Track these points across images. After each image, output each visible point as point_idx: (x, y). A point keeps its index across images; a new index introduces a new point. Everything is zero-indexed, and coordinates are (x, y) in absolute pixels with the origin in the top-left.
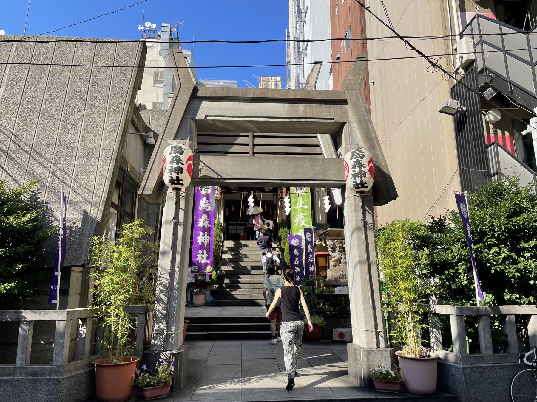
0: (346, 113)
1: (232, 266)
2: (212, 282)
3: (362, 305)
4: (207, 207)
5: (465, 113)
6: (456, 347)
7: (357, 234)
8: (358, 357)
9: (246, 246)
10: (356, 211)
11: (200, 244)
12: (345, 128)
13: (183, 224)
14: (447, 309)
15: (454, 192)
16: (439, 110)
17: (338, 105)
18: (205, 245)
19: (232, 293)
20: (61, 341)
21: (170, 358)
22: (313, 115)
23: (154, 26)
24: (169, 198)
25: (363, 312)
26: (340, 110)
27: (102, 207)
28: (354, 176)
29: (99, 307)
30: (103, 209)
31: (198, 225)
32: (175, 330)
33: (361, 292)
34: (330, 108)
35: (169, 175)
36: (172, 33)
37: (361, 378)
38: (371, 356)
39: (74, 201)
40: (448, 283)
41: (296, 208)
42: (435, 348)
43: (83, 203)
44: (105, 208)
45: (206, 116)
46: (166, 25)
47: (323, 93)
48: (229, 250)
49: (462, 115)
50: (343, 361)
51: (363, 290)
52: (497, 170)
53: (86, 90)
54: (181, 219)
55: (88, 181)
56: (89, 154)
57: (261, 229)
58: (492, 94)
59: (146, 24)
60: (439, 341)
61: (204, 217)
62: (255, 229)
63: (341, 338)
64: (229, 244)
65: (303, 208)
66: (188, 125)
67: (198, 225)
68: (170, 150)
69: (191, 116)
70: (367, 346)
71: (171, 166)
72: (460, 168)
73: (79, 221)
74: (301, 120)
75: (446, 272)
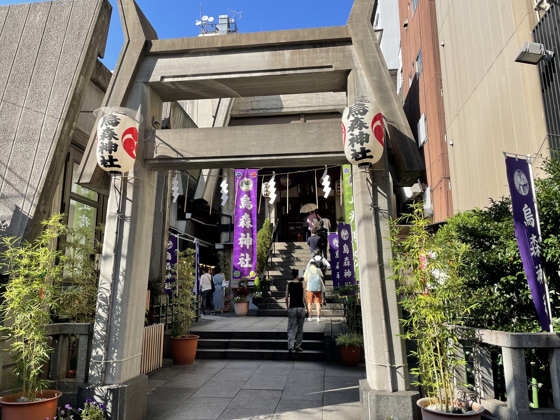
0: (350, 57)
1: (281, 271)
2: (253, 289)
3: (371, 328)
4: (248, 205)
5: (552, 60)
6: (511, 396)
7: (365, 226)
9: (299, 248)
11: (242, 246)
13: (131, 220)
14: (497, 338)
15: (505, 153)
16: (516, 57)
17: (338, 47)
18: (248, 248)
19: (278, 301)
21: (107, 395)
22: (303, 63)
23: (211, 19)
25: (372, 337)
27: (36, 201)
28: (352, 141)
30: (37, 203)
31: (239, 226)
32: (117, 357)
34: (327, 52)
36: (230, 24)
38: (382, 404)
40: (508, 296)
41: (351, 203)
43: (16, 197)
45: (163, 78)
46: (223, 16)
48: (281, 253)
49: (549, 62)
53: (33, 62)
54: (128, 212)
59: (203, 19)
60: (490, 386)
62: (309, 229)
64: (280, 246)
66: (140, 91)
67: (239, 226)
69: (144, 79)
70: (379, 387)
72: (549, 136)
74: (287, 72)
75: (503, 279)
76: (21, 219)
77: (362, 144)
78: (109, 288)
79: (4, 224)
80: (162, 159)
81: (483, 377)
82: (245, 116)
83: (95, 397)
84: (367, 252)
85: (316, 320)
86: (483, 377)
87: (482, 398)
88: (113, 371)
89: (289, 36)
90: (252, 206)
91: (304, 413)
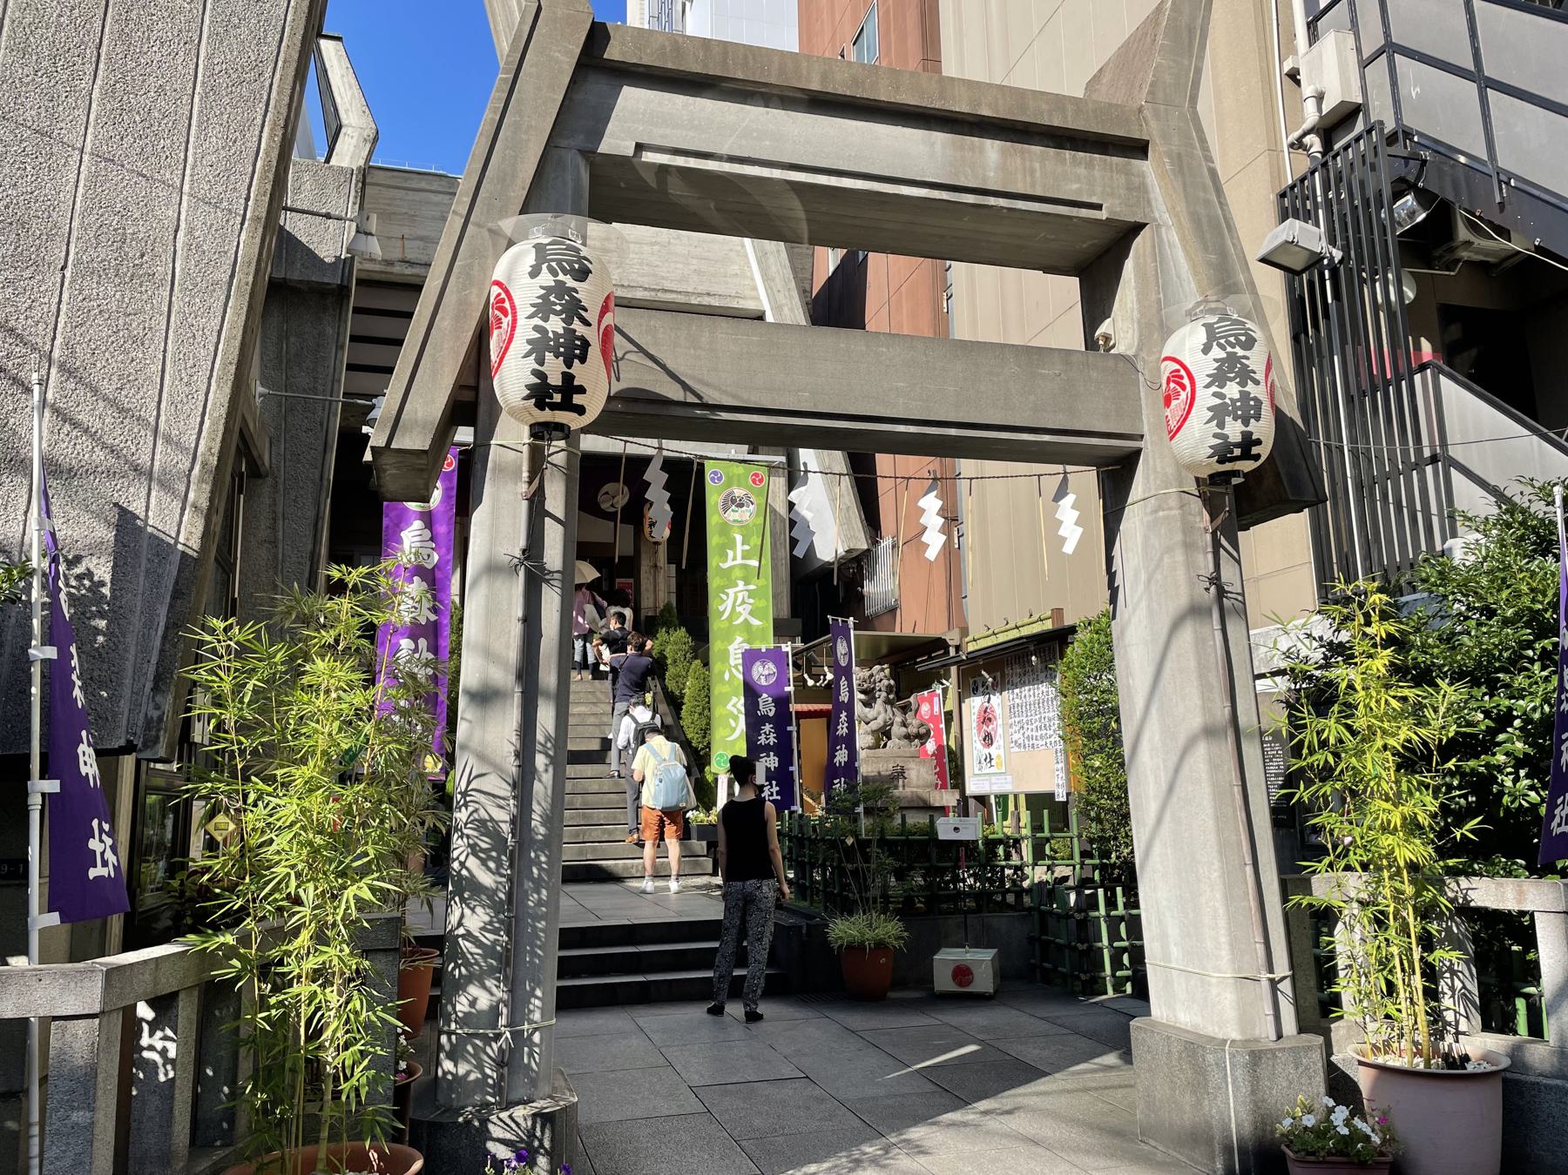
0: (1139, 190)
7: (1195, 632)
8: (1214, 1077)
10: (1188, 546)
12: (1139, 243)
16: (1262, 253)
17: (1115, 159)
20: (78, 1117)
21: (531, 1134)
24: (500, 469)
26: (1122, 179)
27: (199, 494)
29: (229, 939)
30: (204, 504)
33: (1212, 837)
34: (1090, 166)
35: (530, 363)
37: (1228, 1149)
38: (1263, 1071)
39: (65, 463)
41: (725, 566)
42: (1463, 1026)
43: (110, 474)
44: (211, 500)
45: (640, 147)
47: (1070, 107)
50: (1045, 1074)
51: (1219, 831)
52: (1432, 446)
55: (125, 381)
56: (127, 261)
57: (591, 632)
58: (1412, 214)
61: (416, 587)
63: (960, 984)
65: (745, 566)
68: (531, 259)
69: (579, 141)
70: (1243, 1032)
71: (536, 328)
73: (95, 549)
74: (992, 201)
76: (145, 553)
77: (1246, 423)
78: (505, 790)
79: (79, 570)
80: (636, 400)
81: (1464, 987)
82: (383, 277)
83: (490, 1145)
84: (1203, 699)
85: (668, 889)
86: (1464, 987)
87: (1464, 1033)
88: (531, 1055)
89: (1001, 102)
90: (436, 557)
91: (953, 1124)
